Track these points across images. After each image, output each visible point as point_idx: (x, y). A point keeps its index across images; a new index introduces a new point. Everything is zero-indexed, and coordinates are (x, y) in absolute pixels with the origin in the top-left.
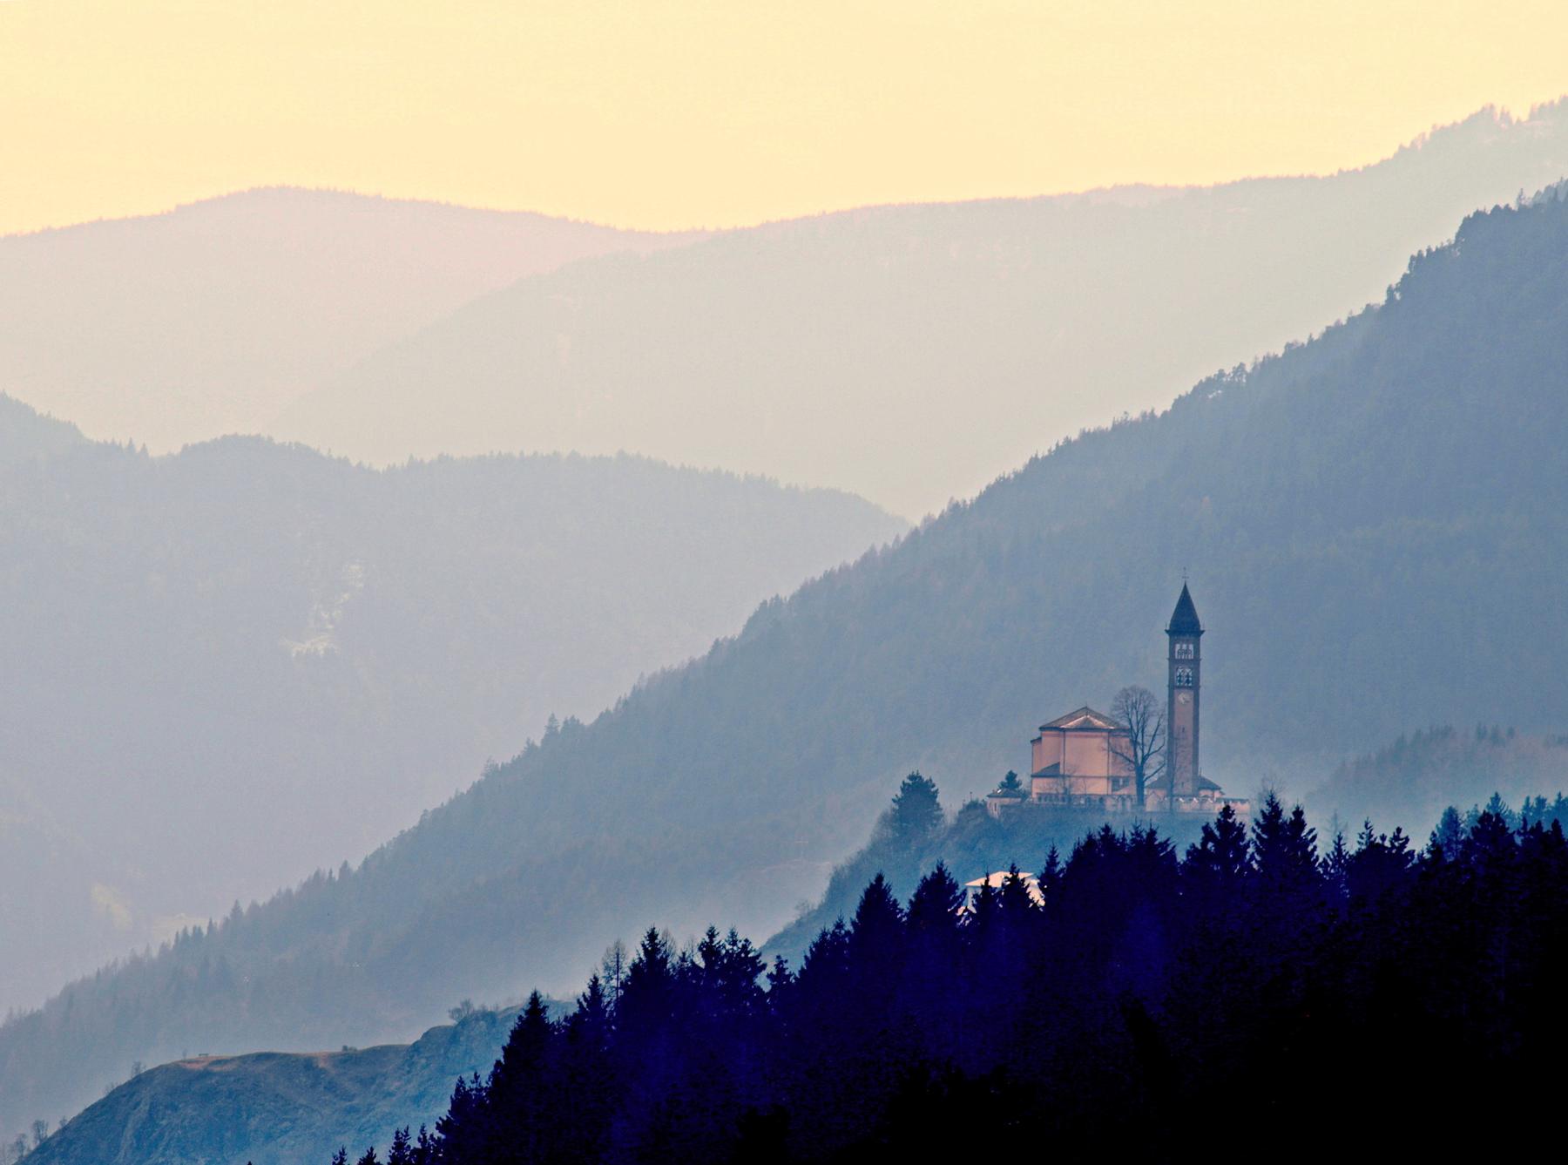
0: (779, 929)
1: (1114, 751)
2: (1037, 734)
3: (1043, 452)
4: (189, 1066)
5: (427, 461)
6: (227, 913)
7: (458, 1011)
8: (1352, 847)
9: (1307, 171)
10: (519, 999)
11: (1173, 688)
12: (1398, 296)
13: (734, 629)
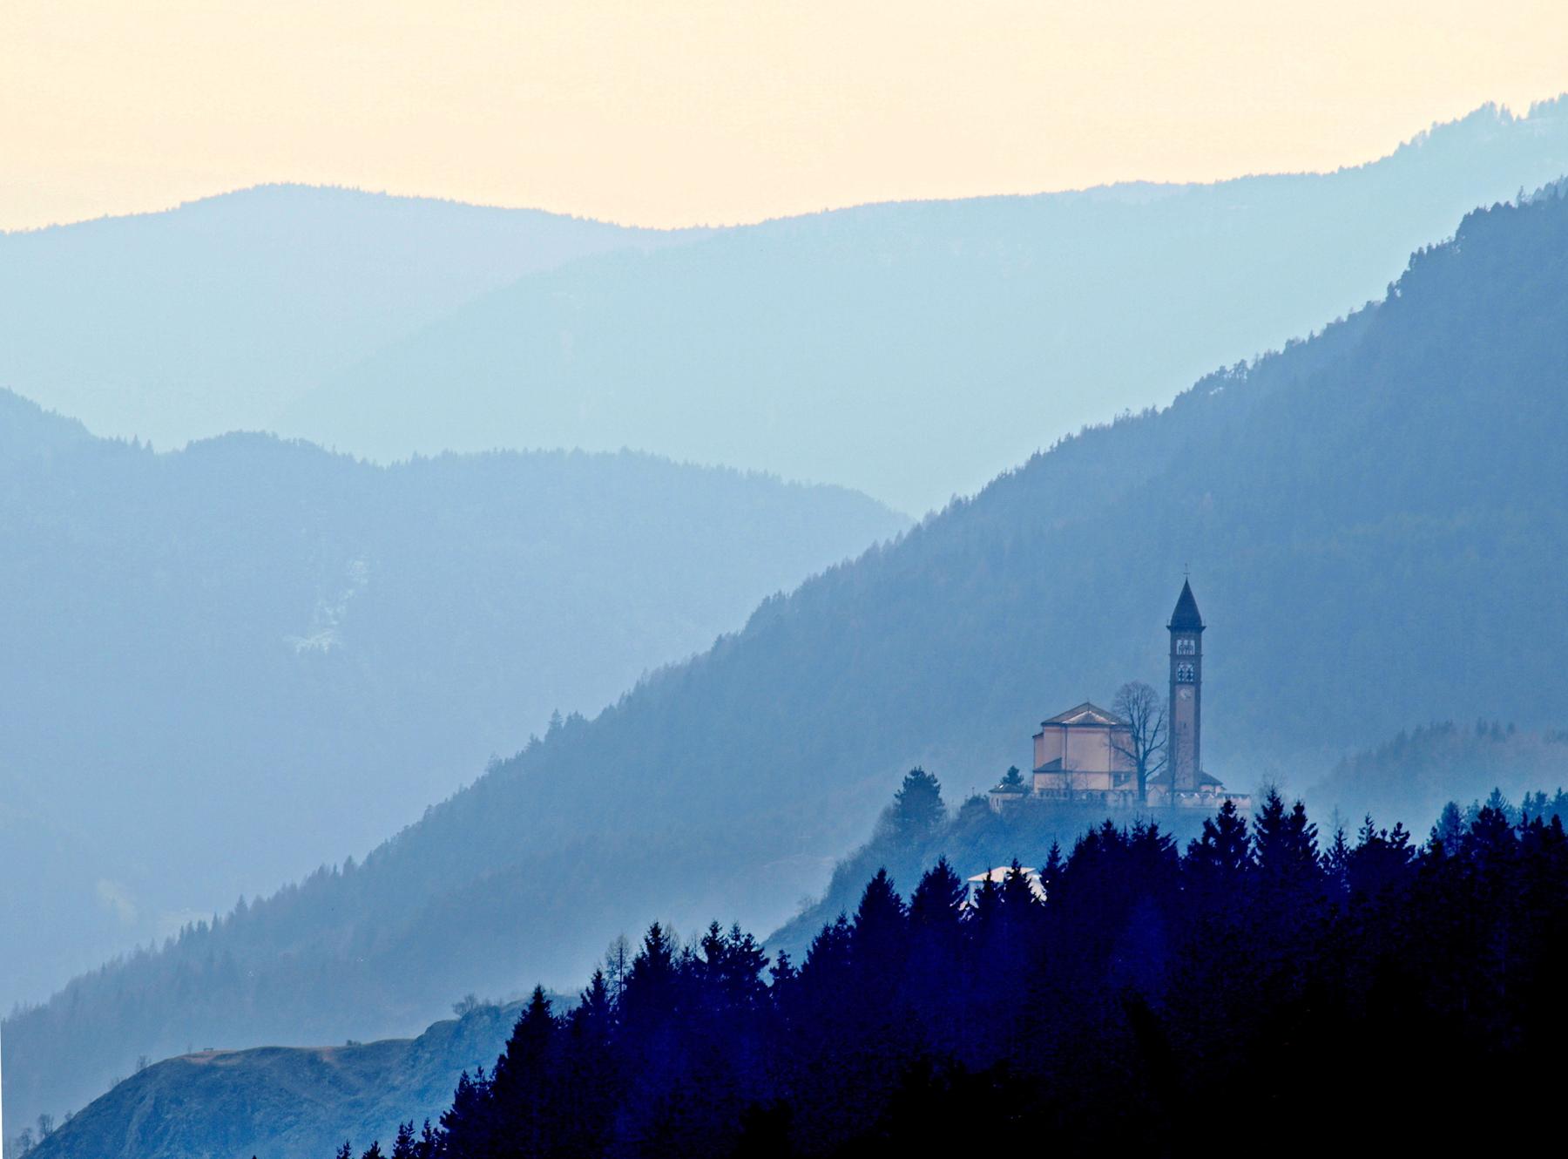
0: (782, 924)
1: (1116, 747)
2: (1039, 729)
3: (1044, 449)
7: (462, 1005)
8: (1353, 842)
10: (522, 994)
11: (1174, 684)
12: (1398, 293)
13: (737, 625)
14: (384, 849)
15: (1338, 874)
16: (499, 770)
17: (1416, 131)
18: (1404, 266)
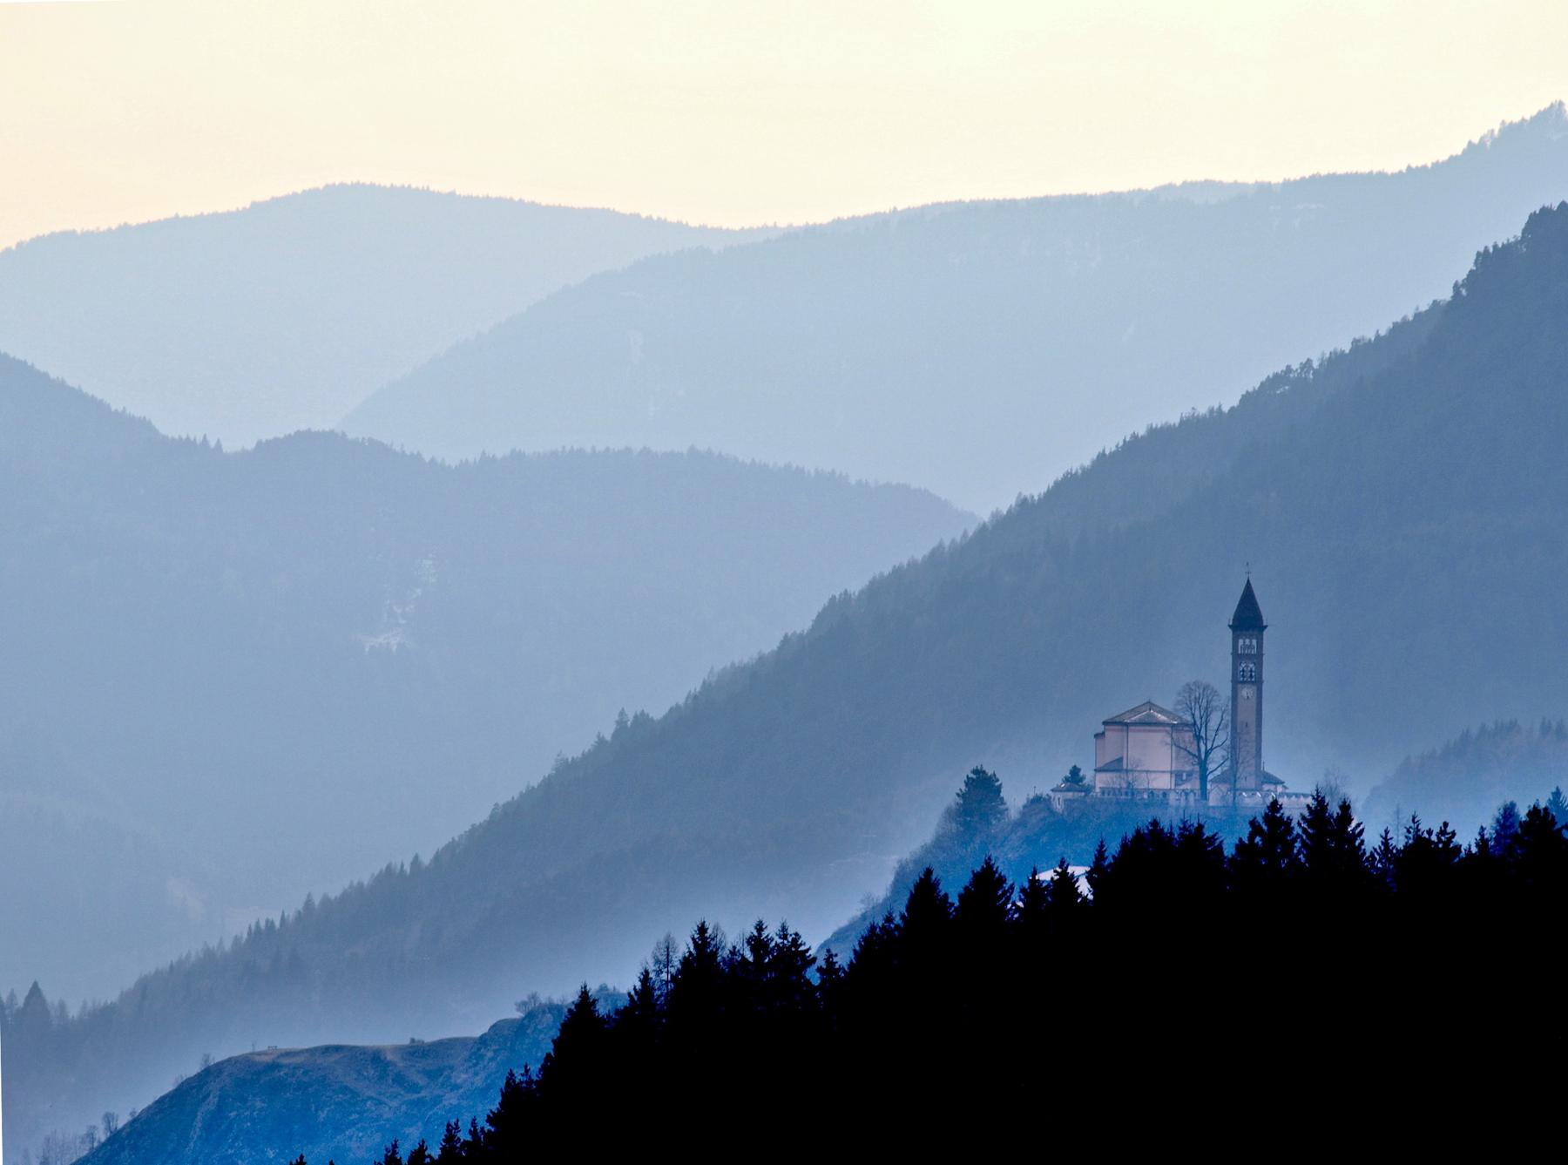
0: (844, 923)
2: (1101, 729)
3: (1110, 448)
4: (258, 1058)
5: (499, 456)
6: (300, 907)
7: (524, 1004)
8: (1399, 841)
9: (1375, 167)
10: (567, 995)
11: (1236, 683)
12: (1464, 292)
13: (802, 623)
14: (451, 847)
15: (1384, 871)
16: (566, 768)
17: (1483, 131)
18: (1469, 264)
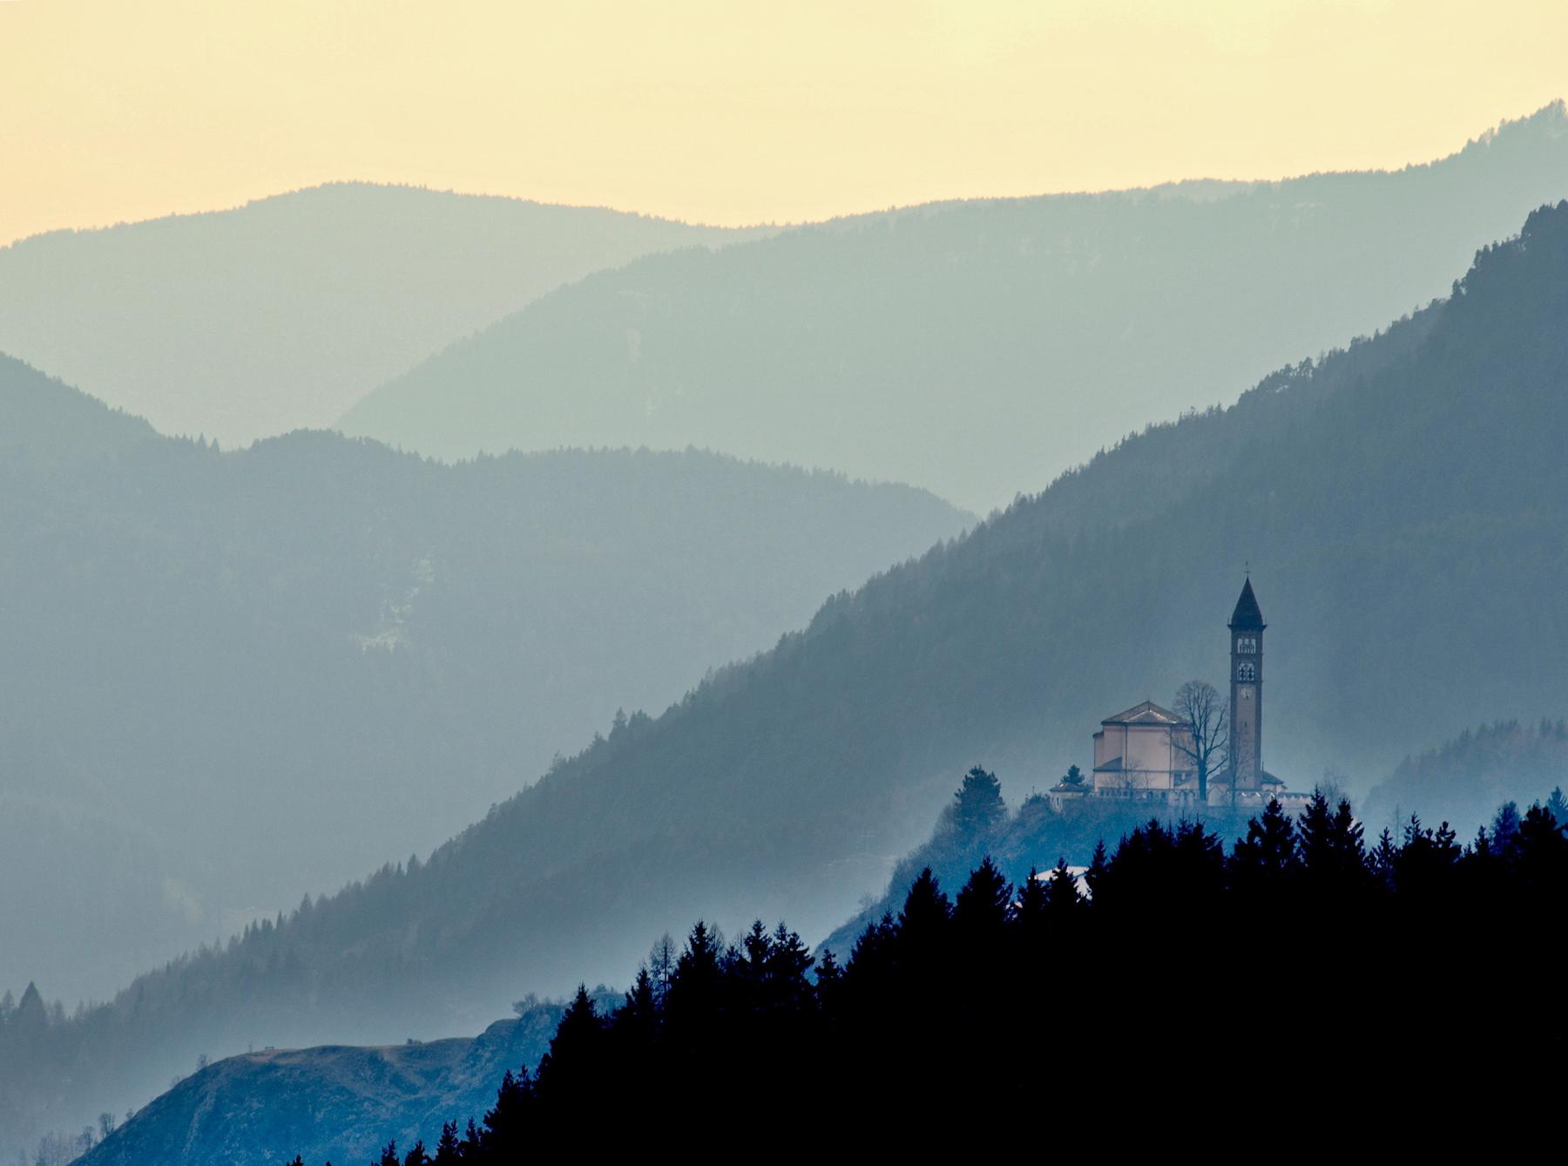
0: (842, 923)
1: (1174, 744)
2: (1100, 728)
3: (1109, 447)
4: (254, 1059)
7: (522, 1004)
8: (1399, 842)
11: (1236, 682)
13: (801, 624)
14: (448, 847)
17: (1484, 129)
18: (1469, 263)
